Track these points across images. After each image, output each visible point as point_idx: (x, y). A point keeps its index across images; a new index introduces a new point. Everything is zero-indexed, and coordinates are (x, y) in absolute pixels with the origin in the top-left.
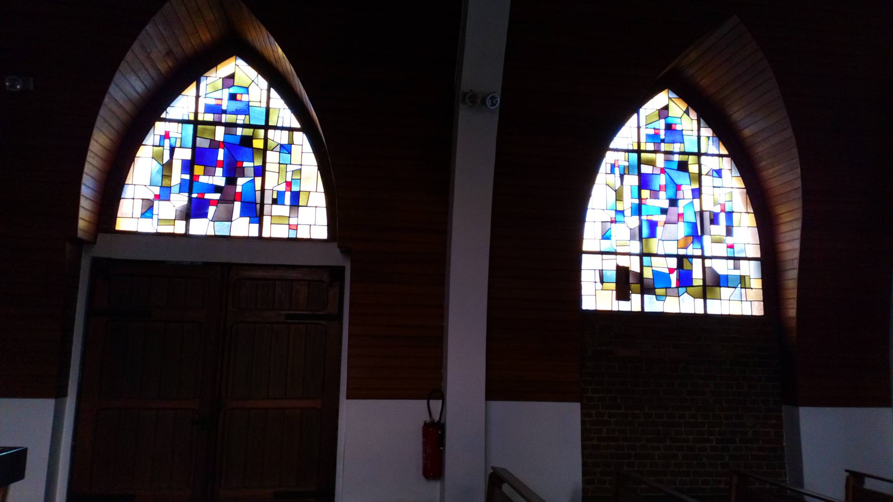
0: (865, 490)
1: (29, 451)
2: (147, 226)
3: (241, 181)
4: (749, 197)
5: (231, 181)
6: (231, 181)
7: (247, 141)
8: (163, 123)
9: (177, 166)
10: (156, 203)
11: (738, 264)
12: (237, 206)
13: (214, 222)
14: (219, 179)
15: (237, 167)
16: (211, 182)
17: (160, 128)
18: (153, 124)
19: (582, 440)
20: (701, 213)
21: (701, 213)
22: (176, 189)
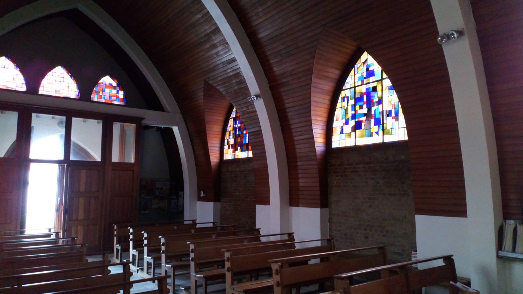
0: (113, 122)
1: (268, 206)
2: (349, 142)
3: (373, 109)
4: (400, 103)
5: (369, 110)
6: (369, 110)
7: (375, 89)
8: (344, 91)
9: (350, 108)
10: (344, 126)
11: (365, 126)
12: (373, 120)
13: (365, 130)
14: (365, 110)
15: (248, 151)
16: (362, 113)
17: (343, 94)
18: (341, 93)
19: (263, 141)
20: (383, 112)
21: (383, 112)
22: (350, 119)
